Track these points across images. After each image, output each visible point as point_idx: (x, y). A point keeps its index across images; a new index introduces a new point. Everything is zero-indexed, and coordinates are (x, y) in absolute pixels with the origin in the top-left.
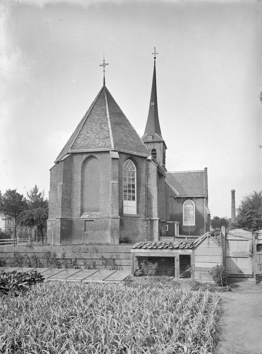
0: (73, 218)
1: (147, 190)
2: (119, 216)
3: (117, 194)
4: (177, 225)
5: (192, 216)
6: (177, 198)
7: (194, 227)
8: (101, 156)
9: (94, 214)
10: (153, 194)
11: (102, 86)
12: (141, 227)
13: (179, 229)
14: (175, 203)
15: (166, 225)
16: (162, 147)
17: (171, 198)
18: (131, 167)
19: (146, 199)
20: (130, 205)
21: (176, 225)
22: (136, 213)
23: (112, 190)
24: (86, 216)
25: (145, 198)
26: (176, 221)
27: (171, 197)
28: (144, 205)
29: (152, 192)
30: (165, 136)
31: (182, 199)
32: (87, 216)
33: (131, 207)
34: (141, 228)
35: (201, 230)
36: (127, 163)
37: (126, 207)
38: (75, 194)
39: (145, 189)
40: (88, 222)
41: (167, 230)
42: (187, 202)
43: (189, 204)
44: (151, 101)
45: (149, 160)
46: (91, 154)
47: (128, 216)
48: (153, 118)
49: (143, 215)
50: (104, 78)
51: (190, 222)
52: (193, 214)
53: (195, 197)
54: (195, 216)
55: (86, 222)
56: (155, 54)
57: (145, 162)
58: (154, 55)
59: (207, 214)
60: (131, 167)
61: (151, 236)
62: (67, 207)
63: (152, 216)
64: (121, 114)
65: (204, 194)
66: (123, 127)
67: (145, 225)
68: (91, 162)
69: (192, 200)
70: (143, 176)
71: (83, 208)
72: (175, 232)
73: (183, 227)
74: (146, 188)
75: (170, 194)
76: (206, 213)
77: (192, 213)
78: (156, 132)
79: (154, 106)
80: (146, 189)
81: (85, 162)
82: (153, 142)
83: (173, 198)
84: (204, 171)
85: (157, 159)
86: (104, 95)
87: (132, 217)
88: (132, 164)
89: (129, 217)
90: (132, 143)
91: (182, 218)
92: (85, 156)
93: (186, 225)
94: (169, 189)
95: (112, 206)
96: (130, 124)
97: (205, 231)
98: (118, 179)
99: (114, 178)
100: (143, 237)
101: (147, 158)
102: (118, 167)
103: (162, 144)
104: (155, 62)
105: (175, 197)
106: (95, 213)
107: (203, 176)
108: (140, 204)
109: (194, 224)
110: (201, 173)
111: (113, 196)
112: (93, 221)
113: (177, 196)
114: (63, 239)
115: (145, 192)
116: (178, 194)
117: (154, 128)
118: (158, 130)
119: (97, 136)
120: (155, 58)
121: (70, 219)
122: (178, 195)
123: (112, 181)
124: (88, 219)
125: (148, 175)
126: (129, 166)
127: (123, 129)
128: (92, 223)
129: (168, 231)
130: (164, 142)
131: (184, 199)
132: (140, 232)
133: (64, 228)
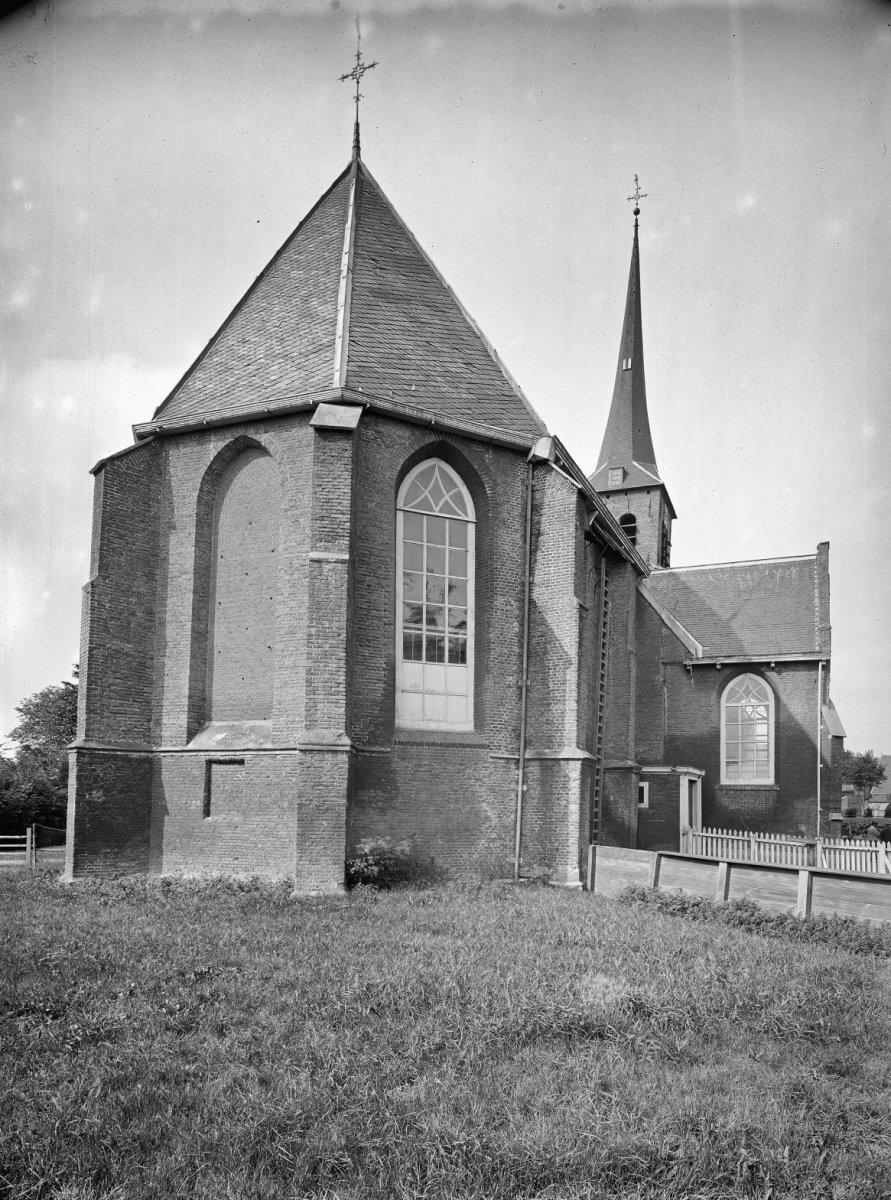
0: (154, 748)
1: (530, 613)
2: (346, 740)
3: (339, 622)
4: (692, 782)
5: (762, 746)
6: (693, 666)
7: (766, 789)
8: (285, 435)
9: (252, 729)
10: (557, 633)
11: (347, 157)
12: (495, 797)
13: (703, 792)
14: (687, 687)
15: (642, 784)
16: (656, 508)
17: (669, 668)
18: (447, 497)
19: (521, 656)
20: (441, 689)
21: (684, 783)
22: (470, 727)
23: (311, 596)
24: (210, 740)
25: (516, 649)
26: (687, 764)
27: (672, 664)
28: (509, 686)
29: (550, 618)
30: (668, 470)
31: (717, 674)
32: (220, 737)
33: (447, 694)
34: (491, 798)
35: (799, 805)
36: (426, 476)
37: (419, 697)
38: (170, 632)
39: (515, 604)
40: (223, 767)
41: (645, 805)
42: (742, 681)
43: (747, 692)
44: (623, 356)
45: (541, 463)
46: (239, 432)
47: (425, 740)
48: (628, 410)
49: (503, 738)
50: (357, 125)
51: (751, 768)
52: (767, 735)
53: (776, 663)
54: (776, 744)
55: (214, 767)
56: (637, 197)
57: (521, 471)
58: (633, 202)
59: (830, 737)
60: (447, 497)
61: (542, 843)
62: (125, 696)
63: (549, 741)
64: (417, 265)
65: (817, 649)
66: (424, 313)
67: (513, 786)
68: (250, 477)
69: (762, 675)
70: (509, 541)
71: (204, 700)
72: (678, 817)
73: (722, 788)
74: (523, 601)
75: (664, 652)
76: (825, 733)
77: (764, 732)
78: (636, 458)
79: (630, 372)
80: (521, 609)
81: (218, 476)
82: (626, 492)
83: (677, 670)
84: (814, 557)
85: (637, 547)
86: (358, 194)
87: (447, 746)
88: (451, 484)
89: (428, 744)
90: (454, 380)
91: (718, 754)
92: (214, 446)
93: (732, 783)
94: (664, 630)
95: (309, 682)
96: (456, 306)
97: (819, 808)
98: (346, 542)
99: (327, 537)
100: (505, 846)
101: (529, 449)
102: (347, 475)
103: (656, 495)
104: (636, 226)
105: (685, 666)
106: (259, 723)
107: (812, 578)
108: (489, 683)
109: (770, 781)
110: (804, 565)
111: (313, 631)
112: (241, 762)
113: (698, 659)
114: (95, 852)
115: (516, 624)
116: (699, 651)
117: (629, 443)
118: (644, 450)
119: (278, 349)
120: (637, 212)
121: (135, 755)
122: (700, 655)
123: (314, 548)
124: (218, 756)
125: (533, 536)
126: (437, 494)
127: (414, 320)
128: (239, 773)
129: (651, 811)
130: (662, 488)
131: (727, 672)
132: (487, 818)
133: (97, 795)
